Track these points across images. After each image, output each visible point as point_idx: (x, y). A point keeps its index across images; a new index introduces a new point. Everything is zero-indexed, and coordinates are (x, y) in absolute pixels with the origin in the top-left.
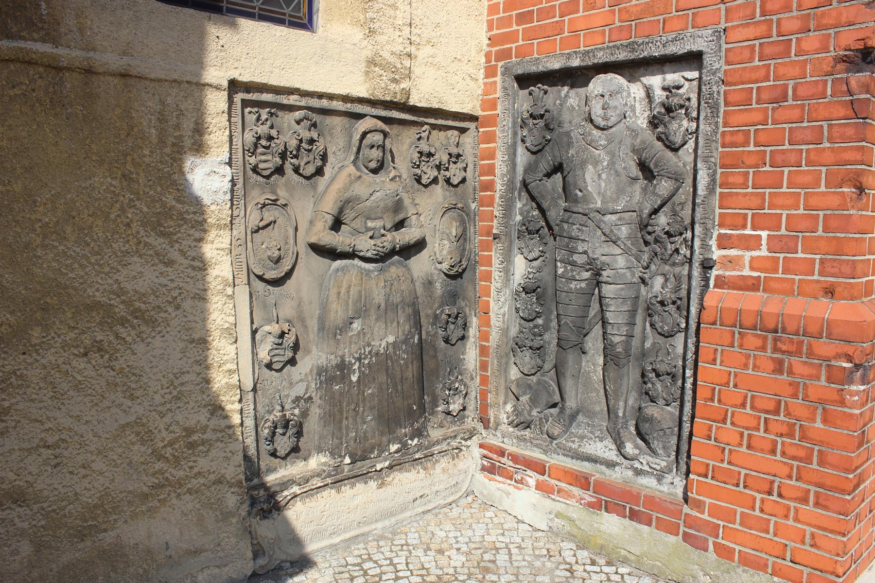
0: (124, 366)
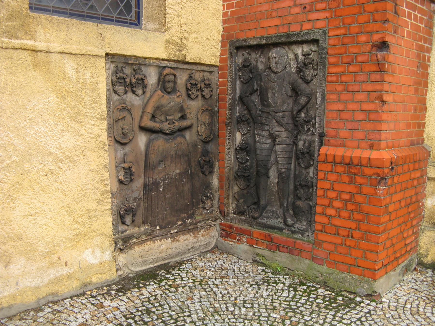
0: (62, 181)
